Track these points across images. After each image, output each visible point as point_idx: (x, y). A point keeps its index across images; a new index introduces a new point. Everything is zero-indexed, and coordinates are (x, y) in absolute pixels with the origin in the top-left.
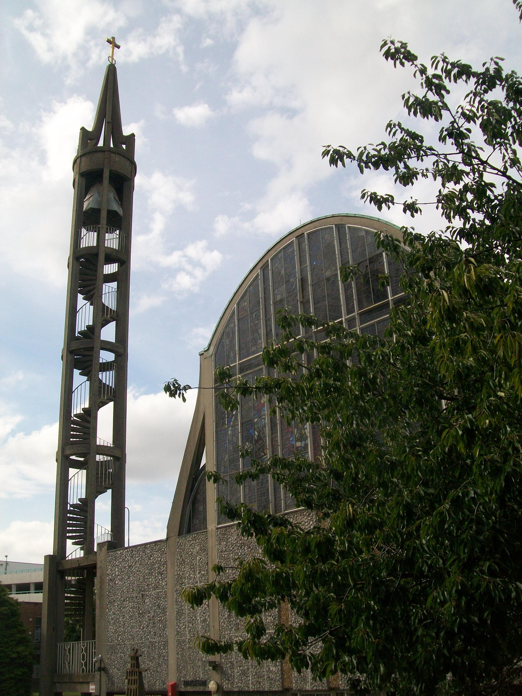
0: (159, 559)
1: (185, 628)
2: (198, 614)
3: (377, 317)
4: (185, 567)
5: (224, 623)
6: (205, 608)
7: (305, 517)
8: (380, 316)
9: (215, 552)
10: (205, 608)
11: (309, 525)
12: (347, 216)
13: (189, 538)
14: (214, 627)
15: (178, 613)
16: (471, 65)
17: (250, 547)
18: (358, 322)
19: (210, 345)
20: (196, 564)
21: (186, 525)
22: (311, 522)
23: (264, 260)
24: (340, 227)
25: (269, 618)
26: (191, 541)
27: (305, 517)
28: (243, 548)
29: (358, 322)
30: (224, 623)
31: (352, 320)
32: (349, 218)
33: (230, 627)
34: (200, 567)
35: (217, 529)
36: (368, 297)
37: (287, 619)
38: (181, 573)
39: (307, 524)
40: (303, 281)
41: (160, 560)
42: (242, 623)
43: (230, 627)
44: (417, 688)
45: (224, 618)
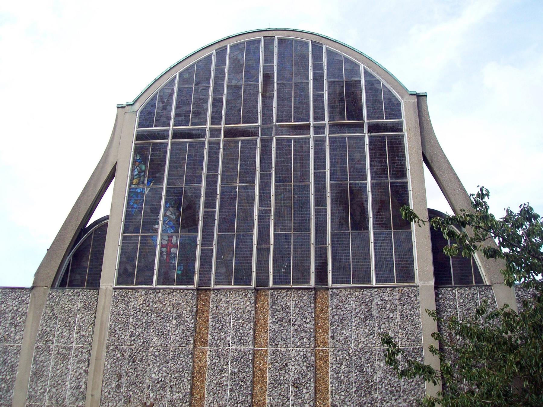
0: (15, 308)
1: (44, 392)
2: (68, 379)
3: (353, 133)
4: (55, 323)
5: (109, 393)
6: (81, 373)
7: (241, 297)
8: (355, 133)
9: (108, 314)
10: (81, 373)
11: (245, 306)
12: (327, 38)
13: (69, 291)
14: (92, 395)
15: (35, 373)
16: (407, 58)
17: (159, 316)
18: (327, 130)
19: (136, 101)
20: (74, 322)
21: (60, 278)
22: (248, 303)
23: (222, 44)
24: (317, 48)
25: (177, 395)
26: (70, 296)
27: (241, 297)
28: (150, 314)
29: (327, 130)
30: (109, 393)
31: (322, 127)
32: (328, 41)
33: (117, 398)
34: (80, 326)
35: (114, 289)
36: (342, 112)
37: (201, 398)
38: (48, 329)
39: (242, 303)
40: (268, 78)
41: (17, 310)
42: (136, 396)
43: (117, 398)
44: (146, 166)
45: (109, 387)
